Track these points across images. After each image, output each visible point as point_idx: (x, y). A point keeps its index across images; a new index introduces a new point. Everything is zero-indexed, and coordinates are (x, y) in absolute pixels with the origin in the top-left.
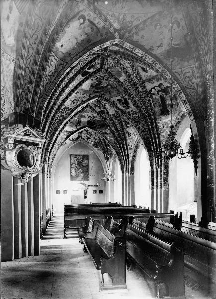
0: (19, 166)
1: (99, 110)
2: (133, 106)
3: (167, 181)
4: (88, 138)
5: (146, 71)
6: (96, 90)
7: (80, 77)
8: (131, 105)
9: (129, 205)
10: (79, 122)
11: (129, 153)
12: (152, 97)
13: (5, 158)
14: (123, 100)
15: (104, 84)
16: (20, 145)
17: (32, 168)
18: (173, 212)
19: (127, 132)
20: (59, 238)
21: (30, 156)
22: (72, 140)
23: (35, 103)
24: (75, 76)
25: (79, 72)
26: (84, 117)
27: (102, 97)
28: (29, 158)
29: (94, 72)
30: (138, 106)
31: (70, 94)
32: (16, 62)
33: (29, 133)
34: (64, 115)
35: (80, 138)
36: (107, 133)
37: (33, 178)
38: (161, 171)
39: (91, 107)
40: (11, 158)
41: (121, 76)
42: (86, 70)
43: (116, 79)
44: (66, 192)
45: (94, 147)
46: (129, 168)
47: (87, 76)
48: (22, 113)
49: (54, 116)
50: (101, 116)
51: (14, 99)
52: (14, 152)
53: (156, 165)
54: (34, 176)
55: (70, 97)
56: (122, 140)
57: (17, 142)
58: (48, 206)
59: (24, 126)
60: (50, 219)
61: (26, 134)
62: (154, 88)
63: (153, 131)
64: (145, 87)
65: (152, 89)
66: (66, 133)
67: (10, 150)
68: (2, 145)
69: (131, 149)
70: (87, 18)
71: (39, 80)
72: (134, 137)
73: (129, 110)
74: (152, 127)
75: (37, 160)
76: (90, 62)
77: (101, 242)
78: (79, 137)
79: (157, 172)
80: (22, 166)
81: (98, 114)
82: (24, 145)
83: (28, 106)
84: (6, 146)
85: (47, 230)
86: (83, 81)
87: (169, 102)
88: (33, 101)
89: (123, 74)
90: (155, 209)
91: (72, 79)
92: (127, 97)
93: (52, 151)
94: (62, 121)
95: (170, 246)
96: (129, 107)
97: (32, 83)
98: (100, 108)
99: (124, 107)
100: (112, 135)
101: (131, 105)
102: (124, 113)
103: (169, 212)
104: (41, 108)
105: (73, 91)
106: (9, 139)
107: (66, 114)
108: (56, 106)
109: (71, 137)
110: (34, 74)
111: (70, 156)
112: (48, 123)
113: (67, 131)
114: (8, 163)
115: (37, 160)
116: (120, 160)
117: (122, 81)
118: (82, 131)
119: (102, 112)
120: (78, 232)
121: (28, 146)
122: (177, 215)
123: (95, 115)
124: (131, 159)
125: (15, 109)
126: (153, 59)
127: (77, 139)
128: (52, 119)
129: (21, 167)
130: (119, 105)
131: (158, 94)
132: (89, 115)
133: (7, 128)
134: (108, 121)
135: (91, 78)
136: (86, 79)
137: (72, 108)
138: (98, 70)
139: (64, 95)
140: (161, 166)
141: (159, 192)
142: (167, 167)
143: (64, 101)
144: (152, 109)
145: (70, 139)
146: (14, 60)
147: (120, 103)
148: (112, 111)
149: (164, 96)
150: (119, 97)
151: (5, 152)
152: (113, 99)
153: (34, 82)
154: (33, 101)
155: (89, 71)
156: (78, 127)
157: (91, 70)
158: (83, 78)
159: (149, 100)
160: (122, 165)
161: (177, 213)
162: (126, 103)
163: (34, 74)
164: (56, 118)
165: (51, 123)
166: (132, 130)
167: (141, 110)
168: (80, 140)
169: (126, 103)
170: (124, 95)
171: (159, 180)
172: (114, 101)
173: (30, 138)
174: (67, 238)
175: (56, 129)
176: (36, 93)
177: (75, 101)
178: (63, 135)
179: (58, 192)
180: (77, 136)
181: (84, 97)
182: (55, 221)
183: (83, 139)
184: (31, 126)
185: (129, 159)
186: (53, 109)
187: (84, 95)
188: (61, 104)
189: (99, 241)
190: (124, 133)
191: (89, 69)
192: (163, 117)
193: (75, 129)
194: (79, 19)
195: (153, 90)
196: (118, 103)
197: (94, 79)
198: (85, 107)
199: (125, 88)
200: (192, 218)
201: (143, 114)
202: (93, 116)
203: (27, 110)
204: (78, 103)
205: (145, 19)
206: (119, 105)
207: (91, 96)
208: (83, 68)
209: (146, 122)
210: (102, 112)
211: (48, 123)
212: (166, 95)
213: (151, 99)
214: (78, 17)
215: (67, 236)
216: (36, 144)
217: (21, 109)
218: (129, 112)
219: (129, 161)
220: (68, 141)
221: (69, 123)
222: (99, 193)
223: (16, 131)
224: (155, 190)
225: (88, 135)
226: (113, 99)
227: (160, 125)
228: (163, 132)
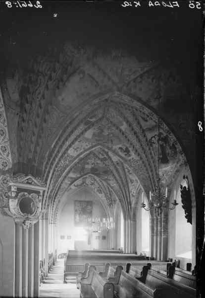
0: (21, 213)
1: (103, 157)
2: (133, 154)
3: (167, 229)
4: (92, 184)
5: (147, 121)
6: (98, 139)
7: (82, 127)
8: (133, 153)
9: (131, 251)
10: (83, 169)
11: (131, 200)
12: (152, 146)
13: (8, 205)
14: (124, 148)
15: (106, 133)
16: (22, 193)
17: (33, 215)
18: (172, 260)
19: (130, 179)
20: (59, 283)
21: (32, 204)
22: (77, 186)
23: (36, 153)
24: (78, 125)
25: (82, 121)
26: (88, 164)
27: (104, 146)
28: (30, 206)
29: (97, 122)
30: (139, 155)
31: (73, 143)
32: (20, 116)
33: (30, 182)
34: (67, 162)
35: (85, 184)
36: (110, 180)
37: (33, 224)
38: (161, 219)
39: (94, 154)
40: (13, 204)
41: (122, 125)
42: (88, 119)
43: (117, 128)
44: (69, 237)
45: (98, 193)
46: (132, 217)
47: (89, 125)
48: (25, 162)
49: (58, 163)
50: (104, 163)
51: (18, 150)
52: (17, 200)
53: (156, 213)
54: (34, 222)
55: (73, 146)
56: (124, 186)
57: (19, 190)
58: (51, 250)
59: (26, 175)
60: (54, 264)
61: (28, 183)
62: (154, 137)
63: (153, 178)
64: (145, 136)
65: (152, 138)
66: (70, 179)
67: (12, 198)
68: (6, 193)
69: (133, 196)
70: (86, 72)
71: (41, 132)
72: (136, 186)
73: (130, 158)
74: (153, 175)
75: (38, 208)
76: (93, 112)
77: (96, 287)
78: (83, 183)
79: (157, 219)
80: (23, 213)
81: (102, 161)
82: (26, 193)
83: (31, 157)
84: (9, 194)
85: (49, 275)
86: (86, 130)
87: (168, 151)
88: (35, 152)
89: (125, 123)
90: (154, 256)
91: (75, 128)
92: (128, 146)
93: (56, 198)
94: (65, 169)
95: (153, 291)
96: (130, 155)
97: (34, 134)
98: (103, 155)
99: (126, 155)
100: (115, 181)
101: (133, 153)
102: (126, 161)
103: (168, 260)
104: (43, 158)
105: (76, 139)
106: (12, 187)
107: (70, 162)
108: (60, 155)
109: (75, 183)
110: (36, 126)
111: (76, 201)
112: (52, 171)
113: (71, 178)
114: (11, 210)
115: (38, 208)
116: (123, 207)
117: (124, 130)
118: (86, 178)
119: (105, 159)
120: (77, 278)
121: (29, 194)
122: (174, 263)
123: (99, 162)
124: (133, 206)
125: (19, 160)
126: (149, 111)
127: (81, 185)
128: (56, 167)
129: (22, 214)
130: (120, 153)
131: (158, 143)
132: (93, 162)
133: (11, 177)
134: (112, 168)
135: (94, 127)
136: (89, 128)
137: (75, 155)
138: (100, 119)
139: (68, 143)
140: (161, 213)
141: (56, 248)
142: (166, 216)
143: (67, 149)
144: (152, 158)
145: (74, 185)
146: (18, 114)
147: (121, 151)
148: (115, 159)
149: (164, 145)
150: (120, 146)
151: (9, 200)
152: (114, 147)
153: (36, 133)
154: (35, 152)
155: (91, 120)
156: (82, 173)
157: (93, 120)
158: (86, 127)
159: (149, 149)
160: (124, 212)
161: (175, 261)
162: (127, 151)
163: (36, 126)
164: (59, 166)
165: (54, 170)
166: (134, 177)
167: (141, 158)
168: (85, 186)
169: (127, 151)
170: (125, 144)
171: (159, 228)
172: (115, 149)
173: (33, 187)
174: (66, 283)
175: (60, 176)
176: (37, 144)
177: (78, 149)
178: (67, 181)
179: (62, 237)
180: (81, 182)
181: (87, 146)
182: (59, 266)
183: (88, 185)
184: (33, 175)
185: (131, 205)
186: (57, 157)
187: (87, 144)
188: (65, 153)
189: (94, 286)
190: (127, 181)
191: (91, 118)
192: (163, 165)
193: (78, 176)
194: (79, 74)
195: (153, 139)
196: (119, 151)
197: (96, 127)
198: (89, 154)
199: (126, 137)
200: (189, 265)
201: (143, 162)
202: (97, 163)
203: (29, 160)
204: (81, 151)
205: (142, 72)
206: (120, 153)
207: (94, 144)
208: (85, 118)
209: (147, 170)
210: (105, 159)
211: (52, 171)
212: (166, 144)
213: (151, 148)
214: (78, 71)
215: (67, 281)
216: (38, 193)
217: (24, 159)
218: (130, 160)
219: (131, 208)
220: (72, 187)
221: (73, 170)
222: (103, 239)
223: (19, 180)
224: (155, 237)
225: (92, 182)
226: (114, 147)
227: (161, 174)
228: (163, 180)
